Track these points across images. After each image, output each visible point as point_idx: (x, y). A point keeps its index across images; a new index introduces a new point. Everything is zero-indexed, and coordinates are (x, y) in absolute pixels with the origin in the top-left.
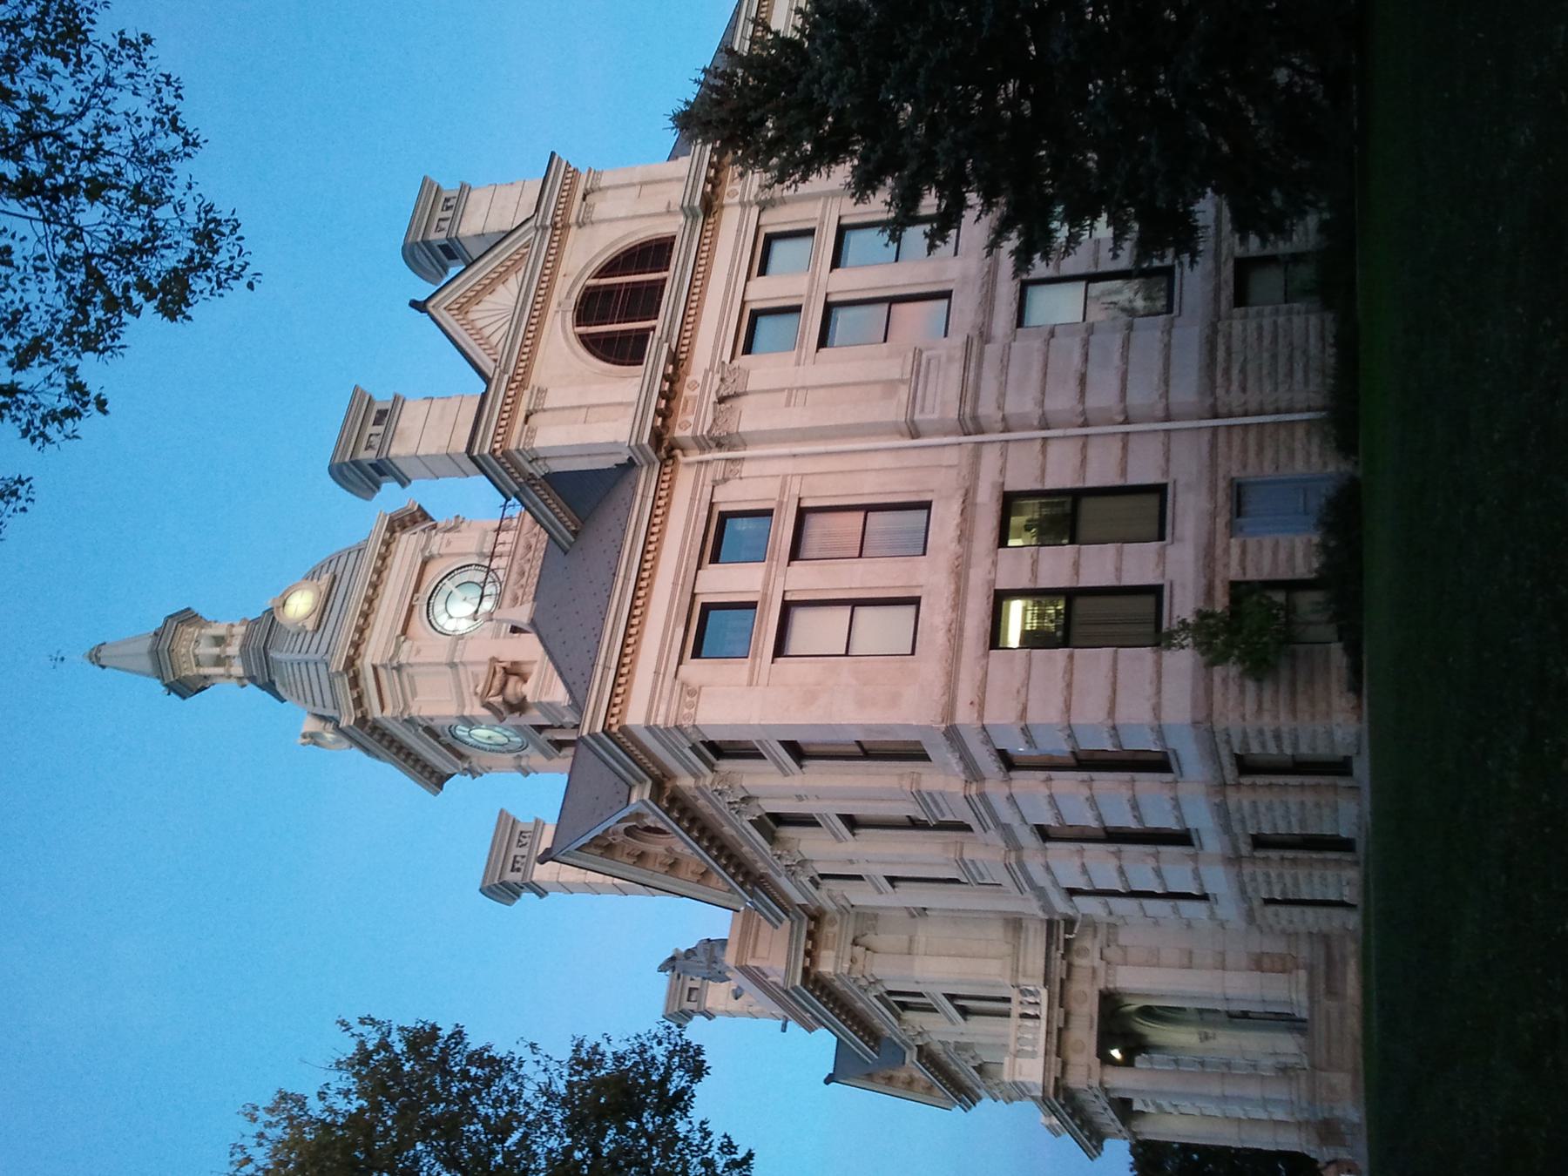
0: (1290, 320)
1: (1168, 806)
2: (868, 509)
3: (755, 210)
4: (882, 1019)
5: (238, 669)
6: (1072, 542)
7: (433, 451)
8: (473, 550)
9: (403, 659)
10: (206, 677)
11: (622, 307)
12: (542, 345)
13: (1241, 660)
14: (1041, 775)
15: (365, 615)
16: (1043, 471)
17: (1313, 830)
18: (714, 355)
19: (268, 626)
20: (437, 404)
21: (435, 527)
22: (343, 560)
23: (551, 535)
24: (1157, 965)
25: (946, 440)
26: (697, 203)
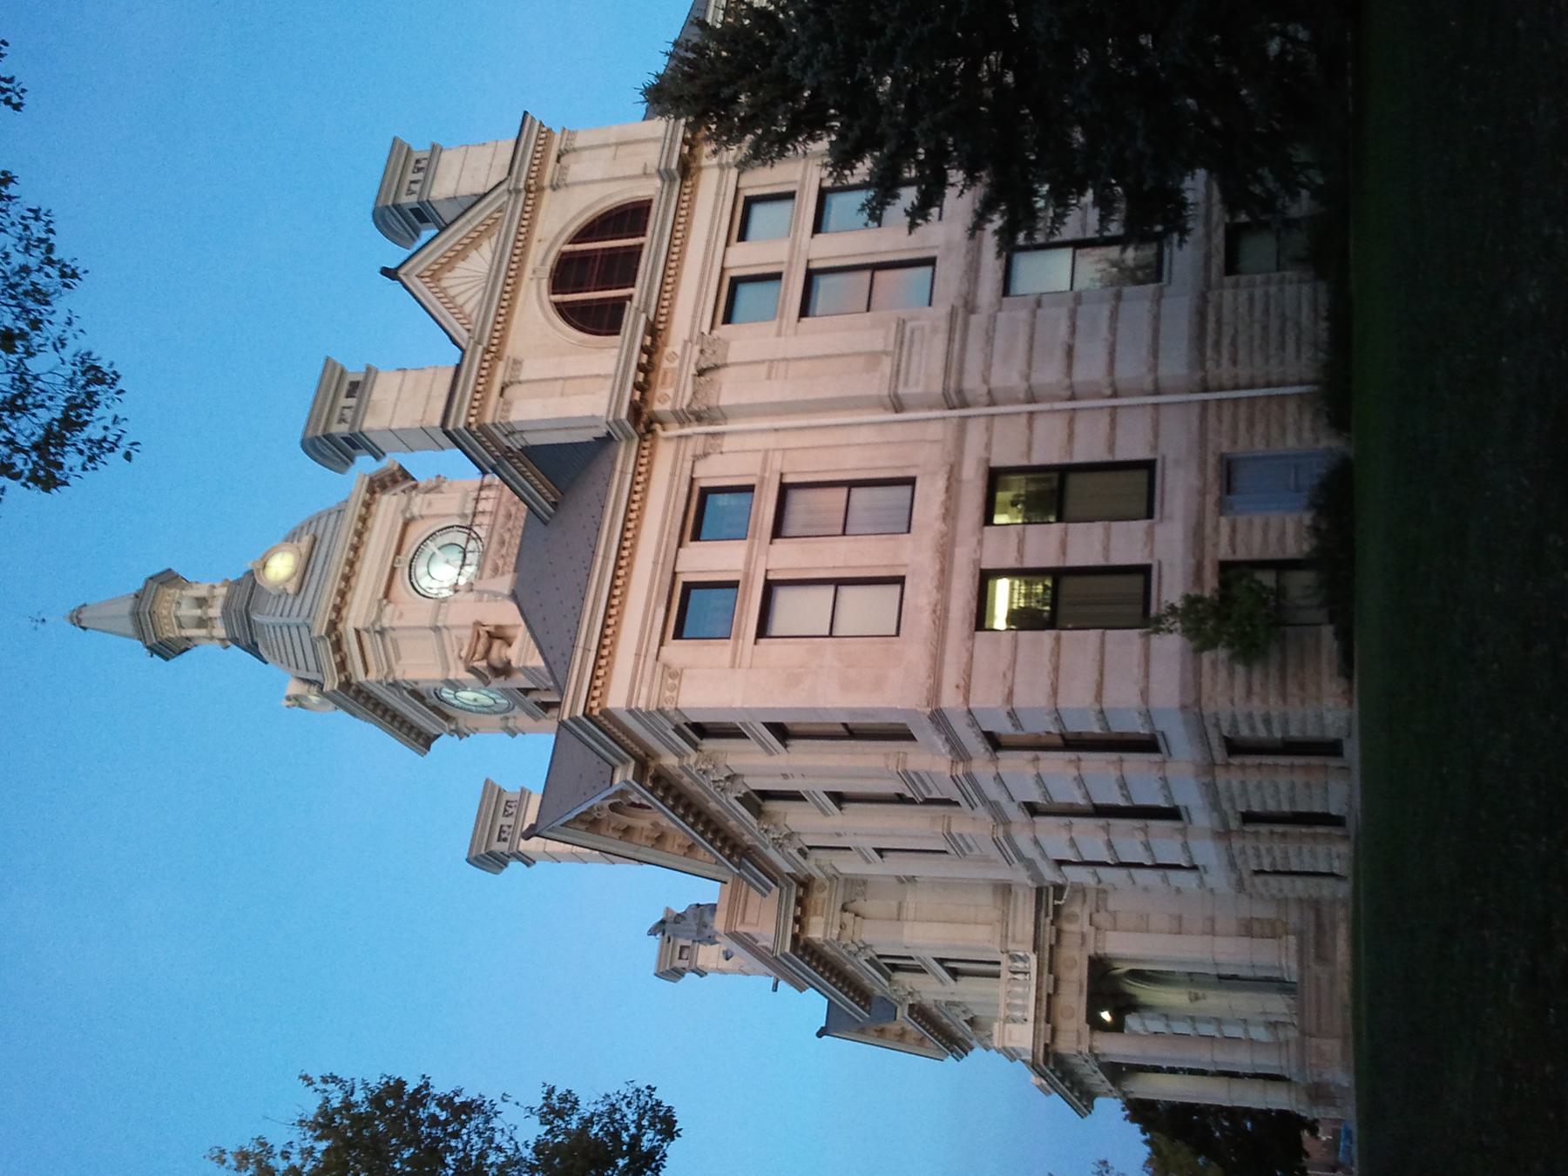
0: (1281, 290)
1: (1156, 785)
2: (851, 484)
4: (873, 980)
5: (220, 631)
6: (1059, 520)
7: (407, 425)
9: (386, 622)
10: (188, 639)
11: (598, 275)
13: (1230, 645)
14: (1029, 755)
18: (692, 328)
20: (411, 375)
21: (415, 487)
24: (1147, 931)
26: (674, 166)
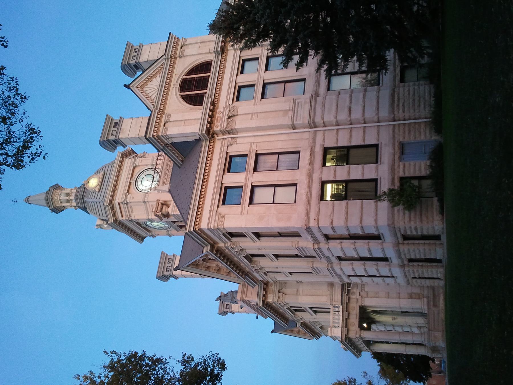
0: (419, 88)
1: (380, 251)
2: (279, 154)
3: (239, 51)
4: (289, 315)
5: (74, 204)
6: (347, 164)
8: (150, 163)
9: (128, 200)
11: (195, 86)
12: (176, 68)
13: (403, 204)
14: (338, 241)
15: (115, 186)
16: (337, 140)
17: (428, 257)
19: (83, 190)
20: (134, 120)
21: (137, 156)
22: (107, 167)
23: (174, 162)
25: (304, 130)
26: (219, 49)
